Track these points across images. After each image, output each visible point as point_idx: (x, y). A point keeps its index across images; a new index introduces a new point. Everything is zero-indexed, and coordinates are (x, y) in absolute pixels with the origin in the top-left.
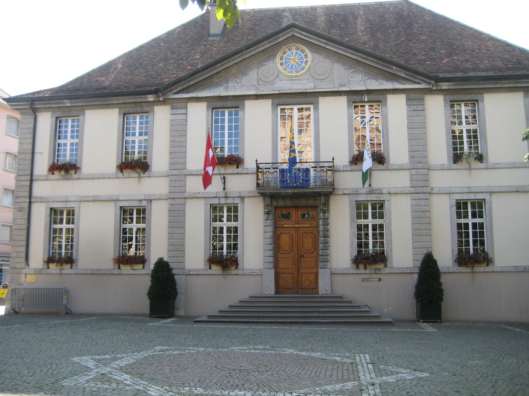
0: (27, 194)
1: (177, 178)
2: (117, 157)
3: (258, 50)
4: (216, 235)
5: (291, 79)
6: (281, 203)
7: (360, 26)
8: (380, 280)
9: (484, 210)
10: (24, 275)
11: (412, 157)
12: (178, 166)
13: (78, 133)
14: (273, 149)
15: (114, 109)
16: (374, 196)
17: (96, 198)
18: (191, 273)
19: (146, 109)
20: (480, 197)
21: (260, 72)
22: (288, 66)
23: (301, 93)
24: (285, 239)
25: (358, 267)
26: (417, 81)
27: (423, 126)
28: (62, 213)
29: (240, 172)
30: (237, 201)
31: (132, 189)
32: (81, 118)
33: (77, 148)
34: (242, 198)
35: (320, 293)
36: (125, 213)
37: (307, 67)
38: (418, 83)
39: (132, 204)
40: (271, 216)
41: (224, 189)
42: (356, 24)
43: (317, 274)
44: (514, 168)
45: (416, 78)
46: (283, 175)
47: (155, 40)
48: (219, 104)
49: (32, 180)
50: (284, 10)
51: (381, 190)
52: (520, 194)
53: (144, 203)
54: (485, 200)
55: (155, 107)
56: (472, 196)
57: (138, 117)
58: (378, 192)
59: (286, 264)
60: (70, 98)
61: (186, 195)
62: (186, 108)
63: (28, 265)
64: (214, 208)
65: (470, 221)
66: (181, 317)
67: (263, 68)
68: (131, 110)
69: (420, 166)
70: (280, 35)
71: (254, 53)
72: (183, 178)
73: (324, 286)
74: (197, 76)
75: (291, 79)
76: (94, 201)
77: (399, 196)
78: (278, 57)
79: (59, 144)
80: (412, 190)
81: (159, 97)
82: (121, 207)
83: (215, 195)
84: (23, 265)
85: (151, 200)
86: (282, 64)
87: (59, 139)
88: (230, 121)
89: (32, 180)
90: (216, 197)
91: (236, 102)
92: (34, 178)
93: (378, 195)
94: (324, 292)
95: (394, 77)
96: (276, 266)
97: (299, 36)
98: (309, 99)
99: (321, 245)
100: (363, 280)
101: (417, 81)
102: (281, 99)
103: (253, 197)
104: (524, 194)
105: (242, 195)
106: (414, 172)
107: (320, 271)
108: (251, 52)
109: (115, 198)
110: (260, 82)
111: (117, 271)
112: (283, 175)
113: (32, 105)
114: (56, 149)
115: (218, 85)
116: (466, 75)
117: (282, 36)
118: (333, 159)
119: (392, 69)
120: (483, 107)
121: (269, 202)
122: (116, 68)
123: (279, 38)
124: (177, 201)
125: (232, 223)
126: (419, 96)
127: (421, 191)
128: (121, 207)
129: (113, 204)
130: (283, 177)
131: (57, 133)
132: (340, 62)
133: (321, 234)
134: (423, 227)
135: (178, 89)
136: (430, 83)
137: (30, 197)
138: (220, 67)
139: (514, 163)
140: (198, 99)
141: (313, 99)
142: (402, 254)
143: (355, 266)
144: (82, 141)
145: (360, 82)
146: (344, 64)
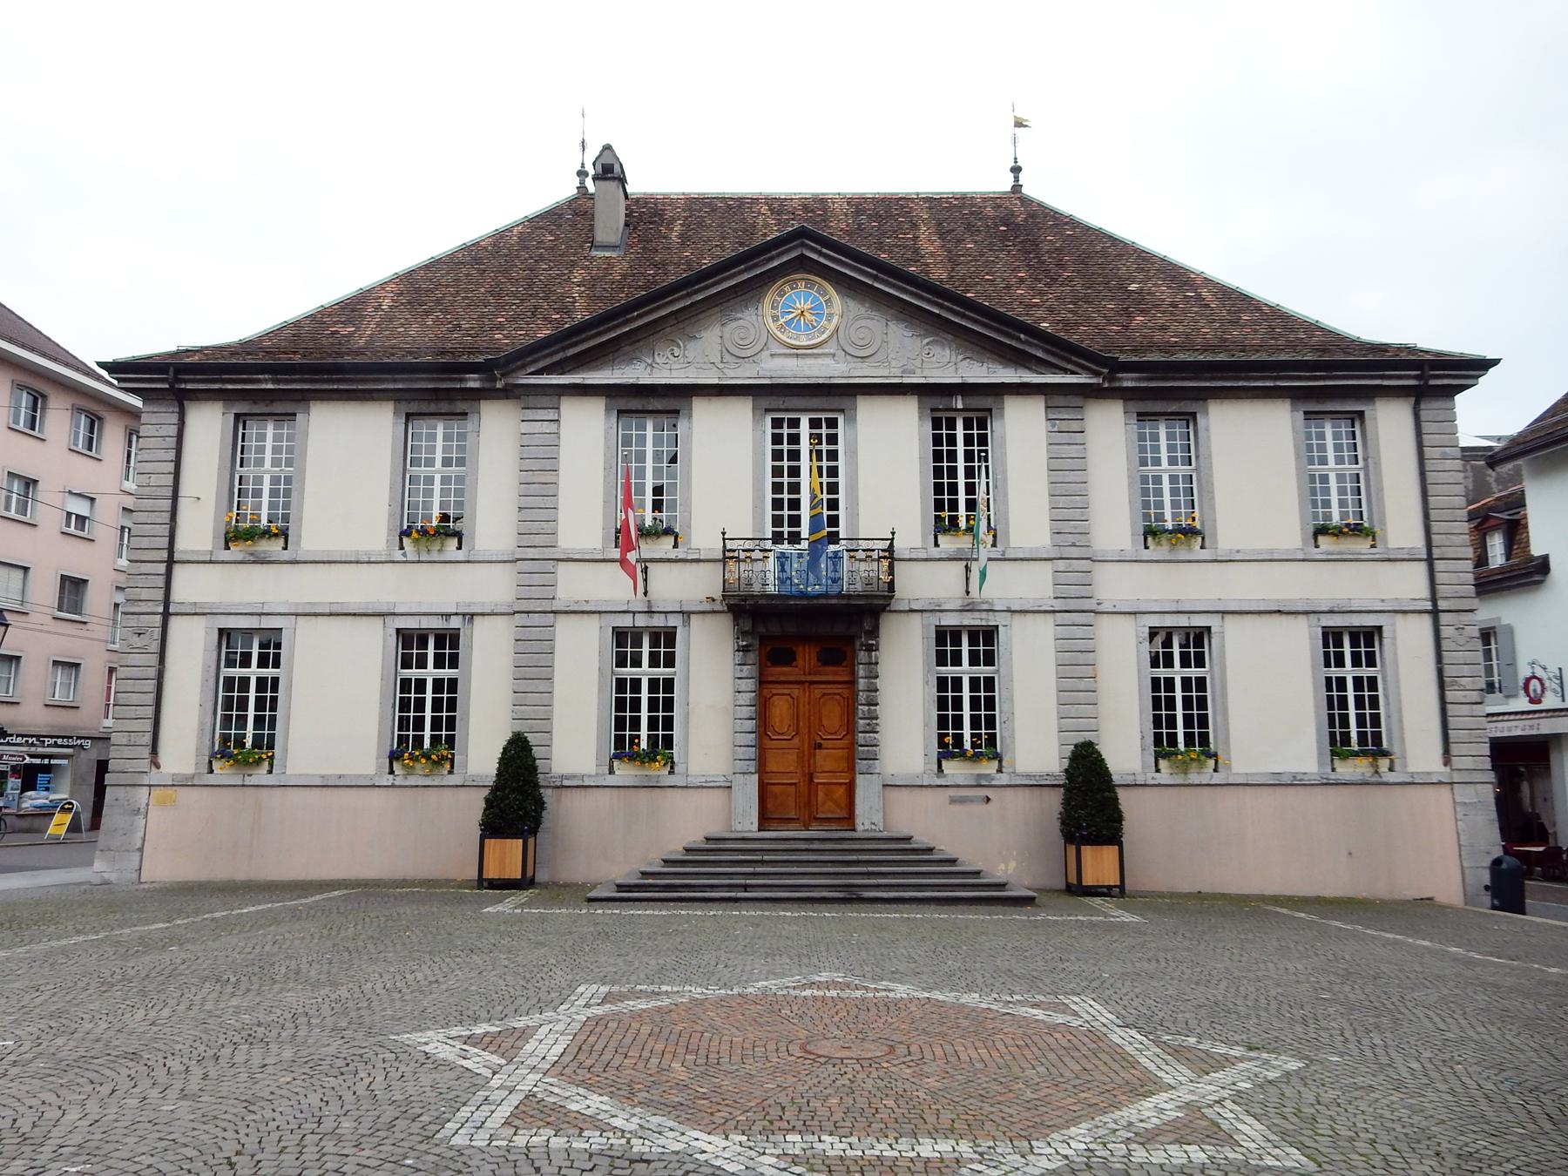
0: (159, 595)
1: (536, 566)
2: (391, 515)
4: (624, 697)
5: (797, 352)
6: (775, 629)
7: (928, 242)
8: (988, 799)
9: (1206, 649)
12: (538, 540)
13: (292, 456)
14: (755, 507)
16: (977, 615)
17: (335, 609)
18: (566, 783)
19: (460, 406)
20: (1199, 621)
21: (726, 336)
24: (781, 709)
26: (1069, 367)
29: (681, 556)
30: (673, 621)
31: (429, 590)
32: (470, 425)
33: (285, 490)
35: (860, 828)
36: (410, 643)
37: (832, 326)
38: (1073, 373)
39: (426, 623)
42: (916, 238)
43: (851, 788)
44: (1389, 560)
45: (1070, 361)
46: (782, 565)
47: (466, 248)
48: (635, 404)
50: (755, 200)
52: (1284, 617)
53: (455, 623)
54: (1209, 628)
56: (1183, 621)
57: (650, 426)
58: (985, 607)
59: (785, 763)
60: (275, 370)
61: (556, 606)
63: (158, 767)
64: (620, 636)
65: (430, 673)
66: (545, 886)
67: (734, 325)
68: (424, 408)
69: (1074, 552)
71: (714, 290)
72: (549, 566)
73: (869, 814)
75: (797, 352)
76: (331, 615)
77: (1029, 616)
78: (767, 300)
80: (1058, 605)
81: (494, 379)
82: (398, 630)
84: (144, 764)
85: (472, 615)
86: (775, 319)
88: (968, 440)
89: (171, 562)
91: (671, 401)
92: (177, 557)
93: (984, 615)
96: (762, 770)
97: (814, 256)
98: (835, 402)
100: (953, 801)
101: (1069, 367)
102: (773, 397)
103: (714, 612)
104: (1291, 617)
105: (685, 609)
106: (1061, 565)
107: (860, 779)
108: (707, 287)
109: (384, 609)
110: (727, 357)
111: (387, 780)
112: (782, 565)
114: (237, 491)
115: (631, 360)
116: (1172, 359)
119: (1018, 339)
120: (1207, 429)
121: (747, 626)
122: (377, 309)
124: (536, 619)
125: (662, 669)
126: (1077, 401)
128: (398, 630)
129: (378, 621)
130: (783, 570)
131: (237, 452)
132: (903, 320)
133: (862, 697)
134: (1082, 685)
135: (541, 365)
136: (1097, 374)
137: (167, 601)
139: (1272, 551)
141: (843, 402)
142: (1035, 745)
145: (948, 365)
146: (911, 325)
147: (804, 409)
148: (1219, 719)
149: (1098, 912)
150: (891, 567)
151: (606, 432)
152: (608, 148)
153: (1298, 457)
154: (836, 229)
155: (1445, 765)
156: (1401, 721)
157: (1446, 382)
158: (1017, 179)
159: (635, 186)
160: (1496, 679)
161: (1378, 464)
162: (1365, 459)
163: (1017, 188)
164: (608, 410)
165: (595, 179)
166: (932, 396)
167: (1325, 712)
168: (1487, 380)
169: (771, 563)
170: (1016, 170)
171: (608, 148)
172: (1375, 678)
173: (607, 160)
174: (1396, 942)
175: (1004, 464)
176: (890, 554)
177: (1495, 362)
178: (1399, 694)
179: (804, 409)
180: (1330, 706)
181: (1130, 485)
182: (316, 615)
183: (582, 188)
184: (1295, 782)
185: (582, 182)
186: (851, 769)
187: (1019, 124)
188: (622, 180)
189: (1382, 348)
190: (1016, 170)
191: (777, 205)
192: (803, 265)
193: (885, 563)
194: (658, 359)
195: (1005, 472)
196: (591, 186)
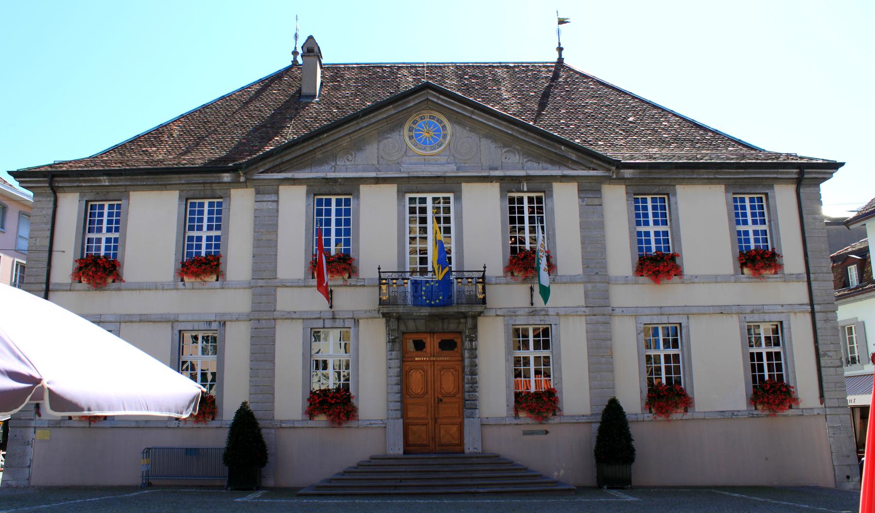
3: (380, 117)
8: (547, 432)
15: (173, 192)
18: (284, 425)
20: (675, 319)
22: (420, 140)
24: (416, 378)
25: (516, 416)
26: (592, 166)
27: (601, 226)
34: (688, 316)
38: (594, 169)
40: (397, 346)
41: (331, 307)
51: (547, 311)
63: (40, 415)
67: (385, 141)
73: (471, 444)
74: (296, 148)
83: (318, 316)
86: (411, 138)
87: (89, 232)
90: (320, 318)
92: (51, 287)
93: (542, 318)
94: (471, 450)
95: (562, 161)
96: (404, 416)
99: (467, 386)
100: (525, 433)
107: (466, 421)
113: (801, 173)
115: (321, 162)
118: (485, 267)
120: (676, 203)
123: (409, 102)
127: (599, 310)
133: (467, 370)
135: (267, 167)
136: (609, 170)
140: (294, 182)
142: (577, 398)
143: (513, 413)
145: (517, 165)
147: (428, 195)
148: (687, 379)
149: (613, 497)
150: (484, 288)
151: (307, 207)
152: (311, 38)
153: (730, 220)
154: (451, 84)
155: (821, 403)
156: (795, 378)
157: (814, 176)
158: (560, 55)
159: (328, 58)
160: (856, 355)
161: (777, 225)
162: (770, 222)
163: (560, 60)
165: (302, 56)
166: (508, 183)
167: (750, 374)
168: (838, 174)
169: (409, 287)
170: (560, 49)
171: (311, 38)
172: (779, 353)
173: (310, 46)
174: (788, 506)
175: (553, 224)
176: (483, 280)
177: (842, 164)
178: (793, 361)
179: (428, 195)
180: (753, 370)
181: (631, 237)
182: (132, 322)
183: (295, 62)
184: (733, 414)
185: (295, 59)
186: (462, 416)
187: (562, 22)
188: (319, 56)
189: (778, 155)
190: (560, 49)
191: (412, 68)
192: (428, 104)
193: (480, 286)
194: (338, 163)
195: (554, 230)
196: (300, 60)
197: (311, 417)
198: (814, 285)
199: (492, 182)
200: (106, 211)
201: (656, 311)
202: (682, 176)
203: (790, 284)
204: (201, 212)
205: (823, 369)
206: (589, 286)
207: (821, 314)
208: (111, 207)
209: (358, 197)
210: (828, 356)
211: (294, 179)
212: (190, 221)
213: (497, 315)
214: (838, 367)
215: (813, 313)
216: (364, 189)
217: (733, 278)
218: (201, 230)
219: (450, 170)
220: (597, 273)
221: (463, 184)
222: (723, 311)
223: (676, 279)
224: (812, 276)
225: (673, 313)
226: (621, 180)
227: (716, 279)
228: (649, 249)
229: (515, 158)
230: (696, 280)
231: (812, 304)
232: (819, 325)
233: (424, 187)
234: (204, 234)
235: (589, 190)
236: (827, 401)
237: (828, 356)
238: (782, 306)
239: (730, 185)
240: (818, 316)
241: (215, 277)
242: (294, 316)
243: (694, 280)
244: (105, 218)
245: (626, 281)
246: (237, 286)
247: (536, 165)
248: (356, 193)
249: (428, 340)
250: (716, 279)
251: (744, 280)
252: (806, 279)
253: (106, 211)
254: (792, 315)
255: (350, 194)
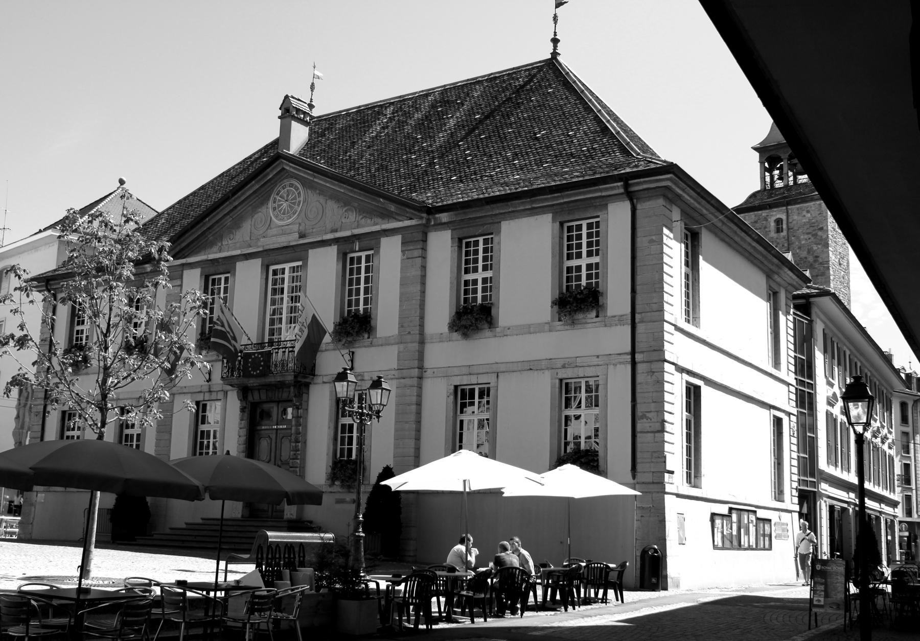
3: (248, 194)
10: (35, 494)
11: (401, 326)
15: (545, 216)
20: (483, 379)
22: (280, 211)
23: (286, 247)
25: (333, 484)
28: (578, 389)
35: (285, 517)
49: (422, 342)
51: (363, 376)
55: (310, 251)
62: (181, 278)
70: (268, 170)
74: (187, 235)
79: (568, 268)
86: (274, 209)
87: (466, 273)
90: (201, 392)
91: (228, 265)
95: (386, 215)
102: (270, 257)
113: (626, 186)
115: (212, 244)
117: (271, 171)
123: (268, 174)
131: (466, 260)
138: (209, 222)
140: (191, 266)
143: (330, 482)
144: (605, 259)
157: (645, 186)
158: (555, 47)
163: (555, 54)
164: (554, 220)
170: (555, 41)
190: (555, 41)
197: (333, 484)
198: (640, 328)
199: (330, 245)
200: (584, 232)
201: (465, 371)
202: (497, 212)
203: (613, 328)
204: (579, 237)
205: (638, 435)
206: (402, 346)
207: (645, 365)
208: (590, 226)
209: (234, 275)
210: (647, 418)
211: (190, 264)
212: (568, 245)
213: (324, 383)
214: (658, 432)
215: (634, 364)
216: (240, 265)
217: (547, 327)
218: (581, 257)
219: (293, 239)
220: (409, 333)
221: (310, 251)
222: (531, 367)
223: (487, 333)
224: (638, 316)
225: (481, 371)
226: (441, 226)
227: (528, 329)
228: (475, 299)
229: (353, 217)
230: (508, 332)
231: (633, 353)
232: (639, 378)
233: (280, 258)
234: (584, 262)
235: (416, 242)
236: (639, 475)
237: (647, 418)
238: (598, 357)
239: (557, 211)
240: (640, 368)
241: (594, 314)
242: (185, 391)
243: (508, 332)
244: (584, 241)
245: (441, 339)
246: (387, 342)
247: (369, 221)
248: (376, 247)
249: (275, 409)
250: (528, 329)
251: (559, 328)
252: (629, 321)
253: (584, 232)
254: (611, 367)
255: (228, 272)
